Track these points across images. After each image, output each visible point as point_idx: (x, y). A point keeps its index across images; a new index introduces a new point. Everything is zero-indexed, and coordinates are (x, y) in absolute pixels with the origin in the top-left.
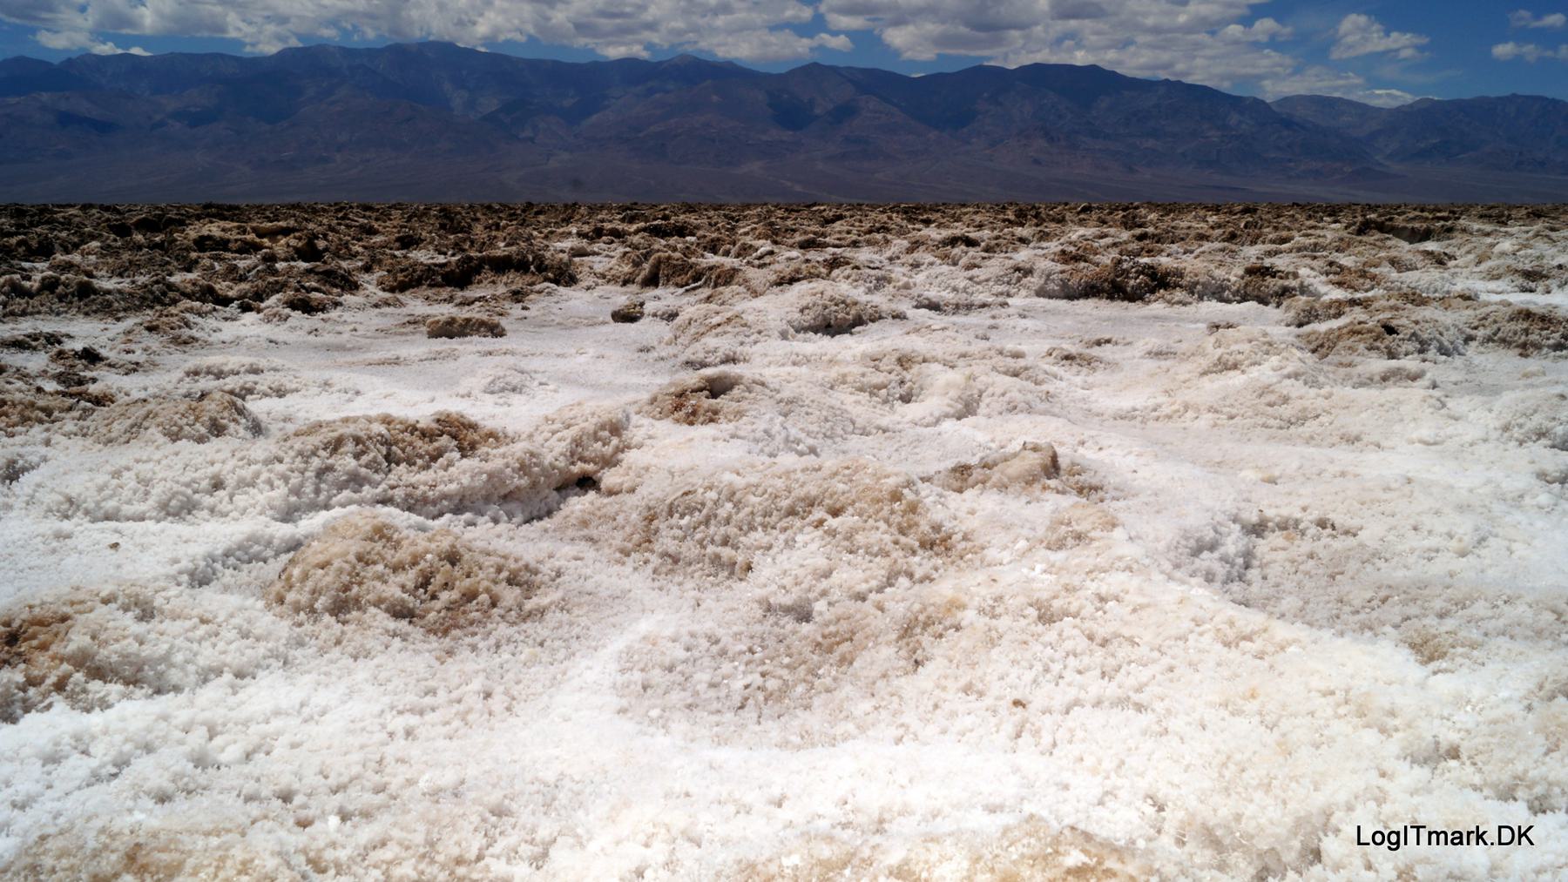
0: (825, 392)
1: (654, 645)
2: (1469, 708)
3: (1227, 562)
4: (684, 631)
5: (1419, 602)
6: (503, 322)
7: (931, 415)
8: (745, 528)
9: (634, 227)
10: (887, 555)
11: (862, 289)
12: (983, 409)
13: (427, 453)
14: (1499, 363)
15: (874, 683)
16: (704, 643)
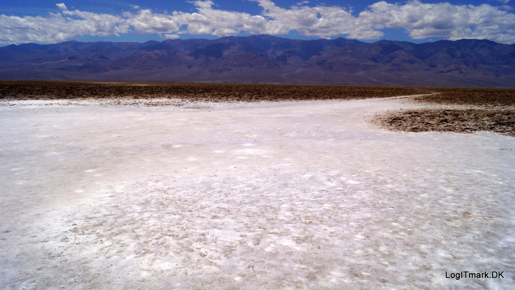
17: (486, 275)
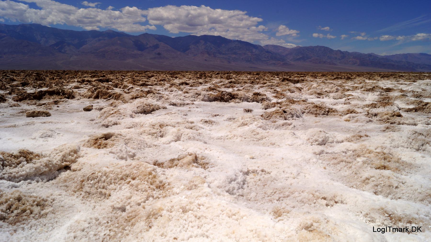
0: (139, 136)
1: (79, 223)
2: (284, 232)
3: (238, 184)
4: (88, 218)
5: (283, 193)
6: (50, 112)
7: (168, 141)
8: (109, 183)
9: (94, 79)
10: (147, 191)
11: (155, 100)
12: (182, 139)
13: (16, 163)
14: (309, 119)
15: (138, 234)
16: (94, 221)
17: (407, 230)
